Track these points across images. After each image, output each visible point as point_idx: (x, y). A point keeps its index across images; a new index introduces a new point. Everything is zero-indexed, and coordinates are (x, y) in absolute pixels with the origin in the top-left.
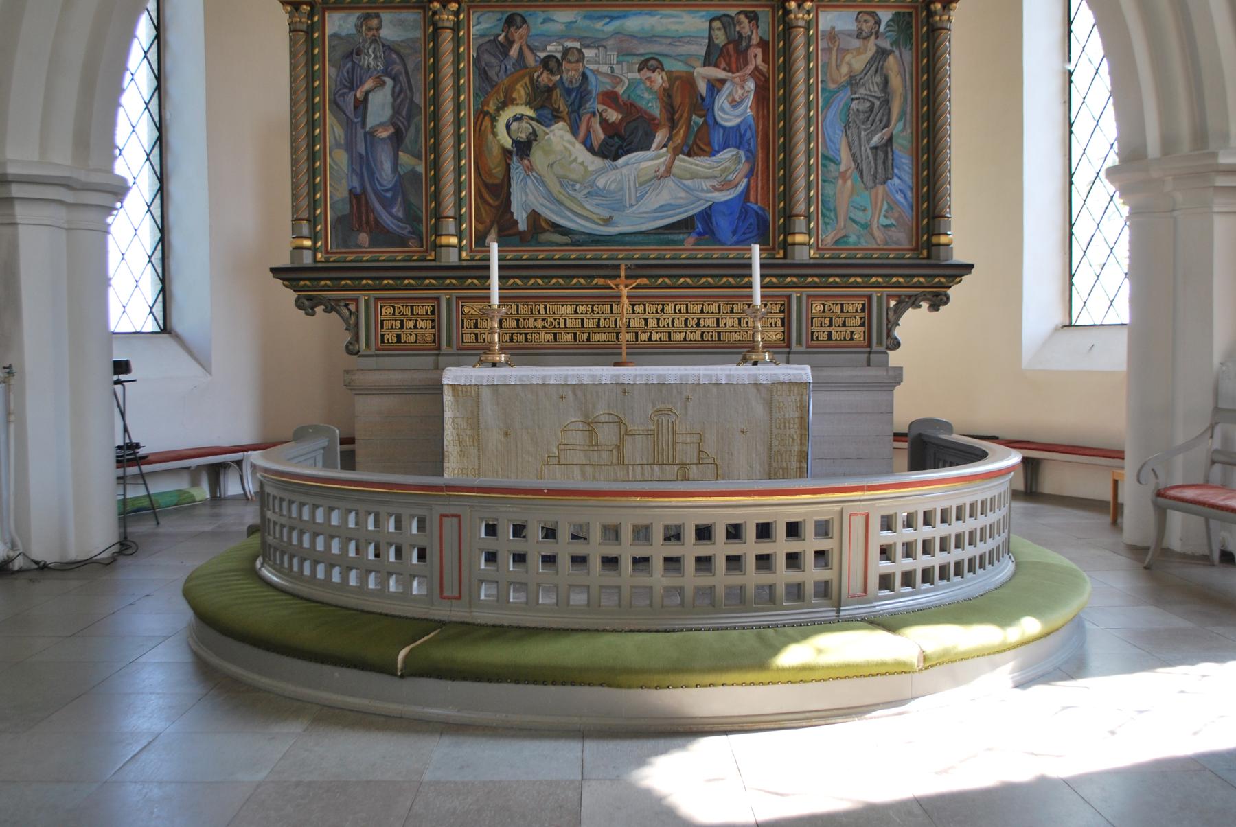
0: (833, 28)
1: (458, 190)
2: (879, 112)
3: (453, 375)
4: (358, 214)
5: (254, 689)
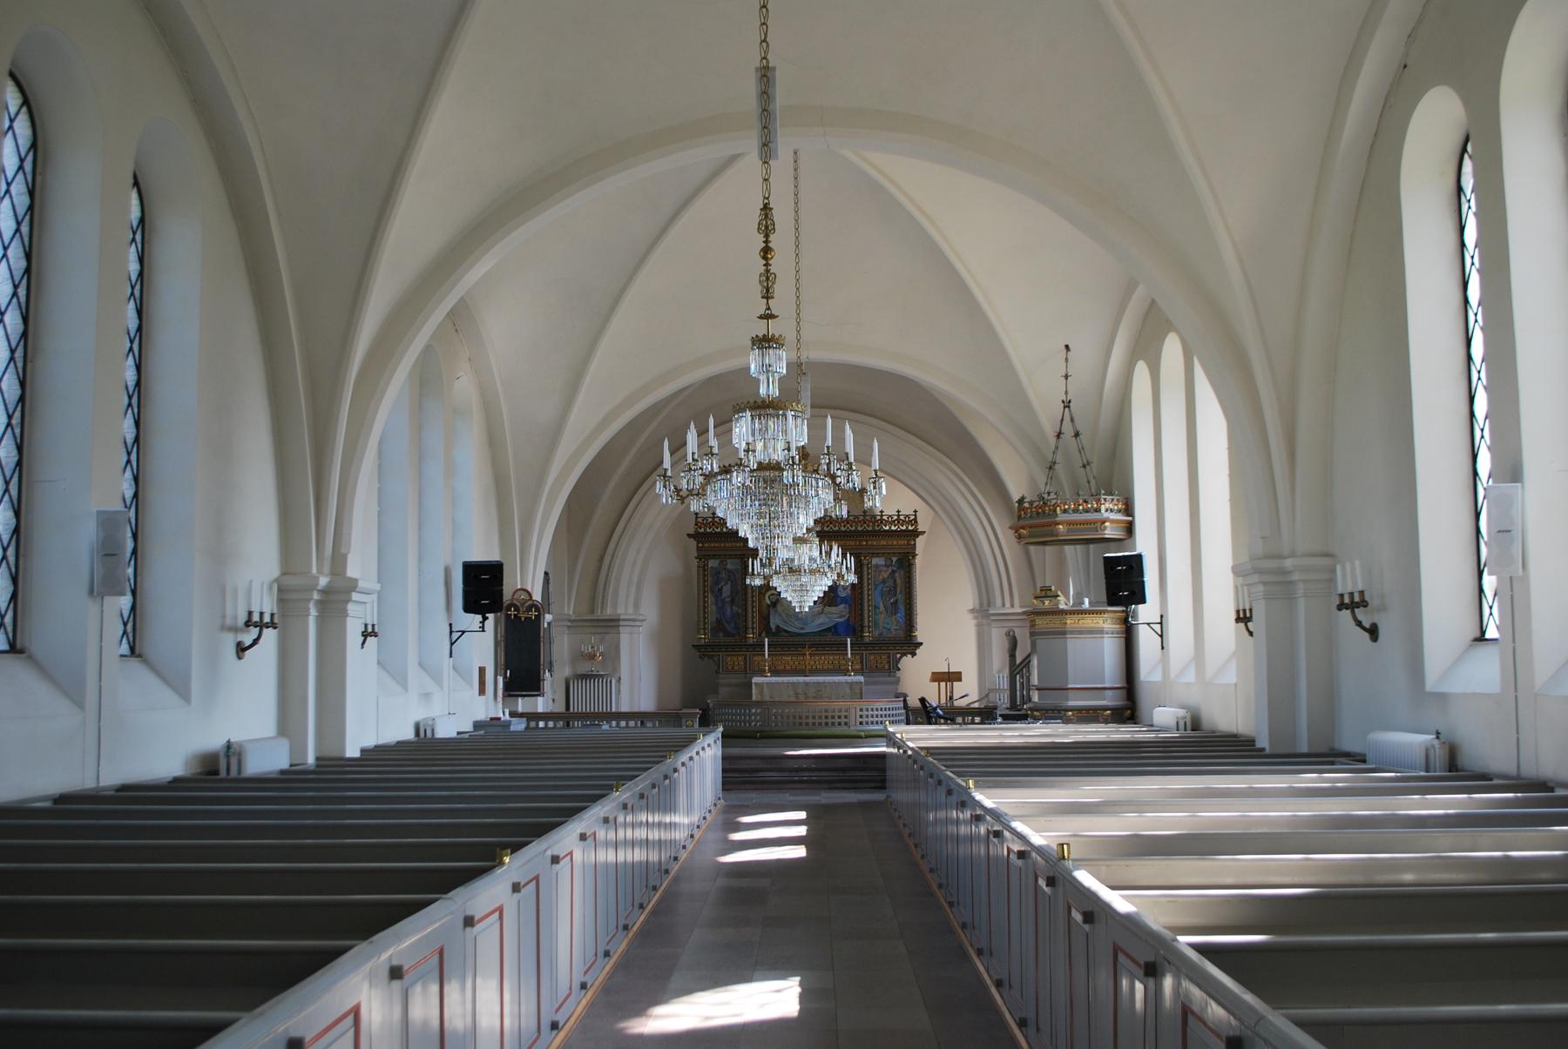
0: (972, 611)
1: (753, 620)
2: (893, 591)
3: (755, 680)
4: (719, 627)
5: (831, 785)
